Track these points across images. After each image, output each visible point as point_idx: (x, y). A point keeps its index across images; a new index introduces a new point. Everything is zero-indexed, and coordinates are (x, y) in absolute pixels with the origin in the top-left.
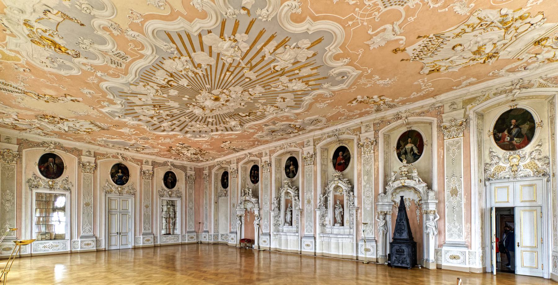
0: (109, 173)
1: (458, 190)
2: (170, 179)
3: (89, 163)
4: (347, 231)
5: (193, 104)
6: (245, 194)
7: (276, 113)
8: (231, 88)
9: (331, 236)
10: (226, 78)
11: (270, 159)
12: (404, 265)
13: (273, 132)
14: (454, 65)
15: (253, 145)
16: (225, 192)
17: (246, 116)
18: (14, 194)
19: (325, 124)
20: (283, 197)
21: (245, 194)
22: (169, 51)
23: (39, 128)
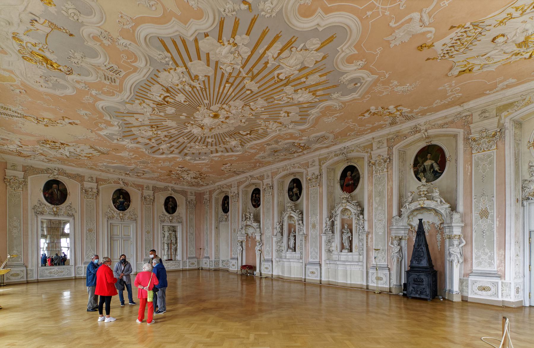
0: (111, 198)
1: (489, 211)
2: (171, 205)
3: (92, 188)
4: (356, 257)
5: (191, 122)
6: (246, 219)
7: (280, 130)
8: (231, 103)
9: (338, 263)
10: (225, 91)
11: (272, 181)
12: (422, 296)
13: (276, 152)
14: (491, 62)
15: (254, 168)
16: (226, 217)
17: (247, 134)
18: (20, 220)
19: (332, 142)
20: (286, 221)
21: (246, 219)
22: (163, 61)
23: (42, 154)
